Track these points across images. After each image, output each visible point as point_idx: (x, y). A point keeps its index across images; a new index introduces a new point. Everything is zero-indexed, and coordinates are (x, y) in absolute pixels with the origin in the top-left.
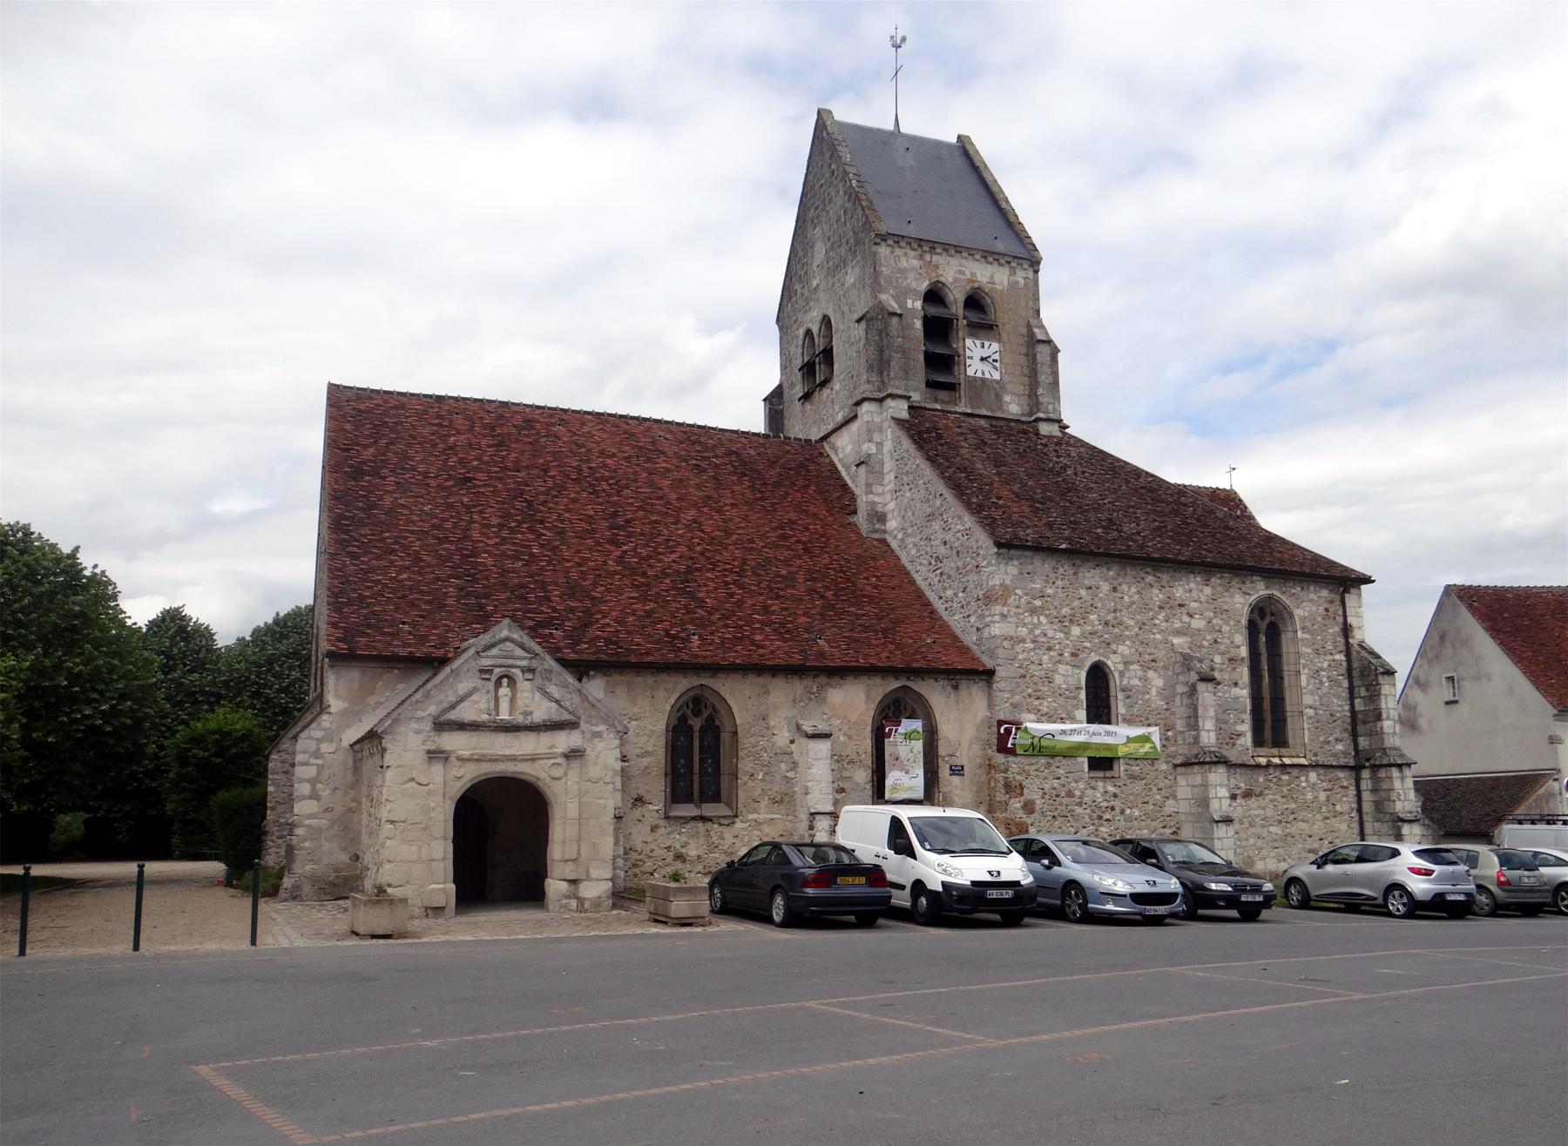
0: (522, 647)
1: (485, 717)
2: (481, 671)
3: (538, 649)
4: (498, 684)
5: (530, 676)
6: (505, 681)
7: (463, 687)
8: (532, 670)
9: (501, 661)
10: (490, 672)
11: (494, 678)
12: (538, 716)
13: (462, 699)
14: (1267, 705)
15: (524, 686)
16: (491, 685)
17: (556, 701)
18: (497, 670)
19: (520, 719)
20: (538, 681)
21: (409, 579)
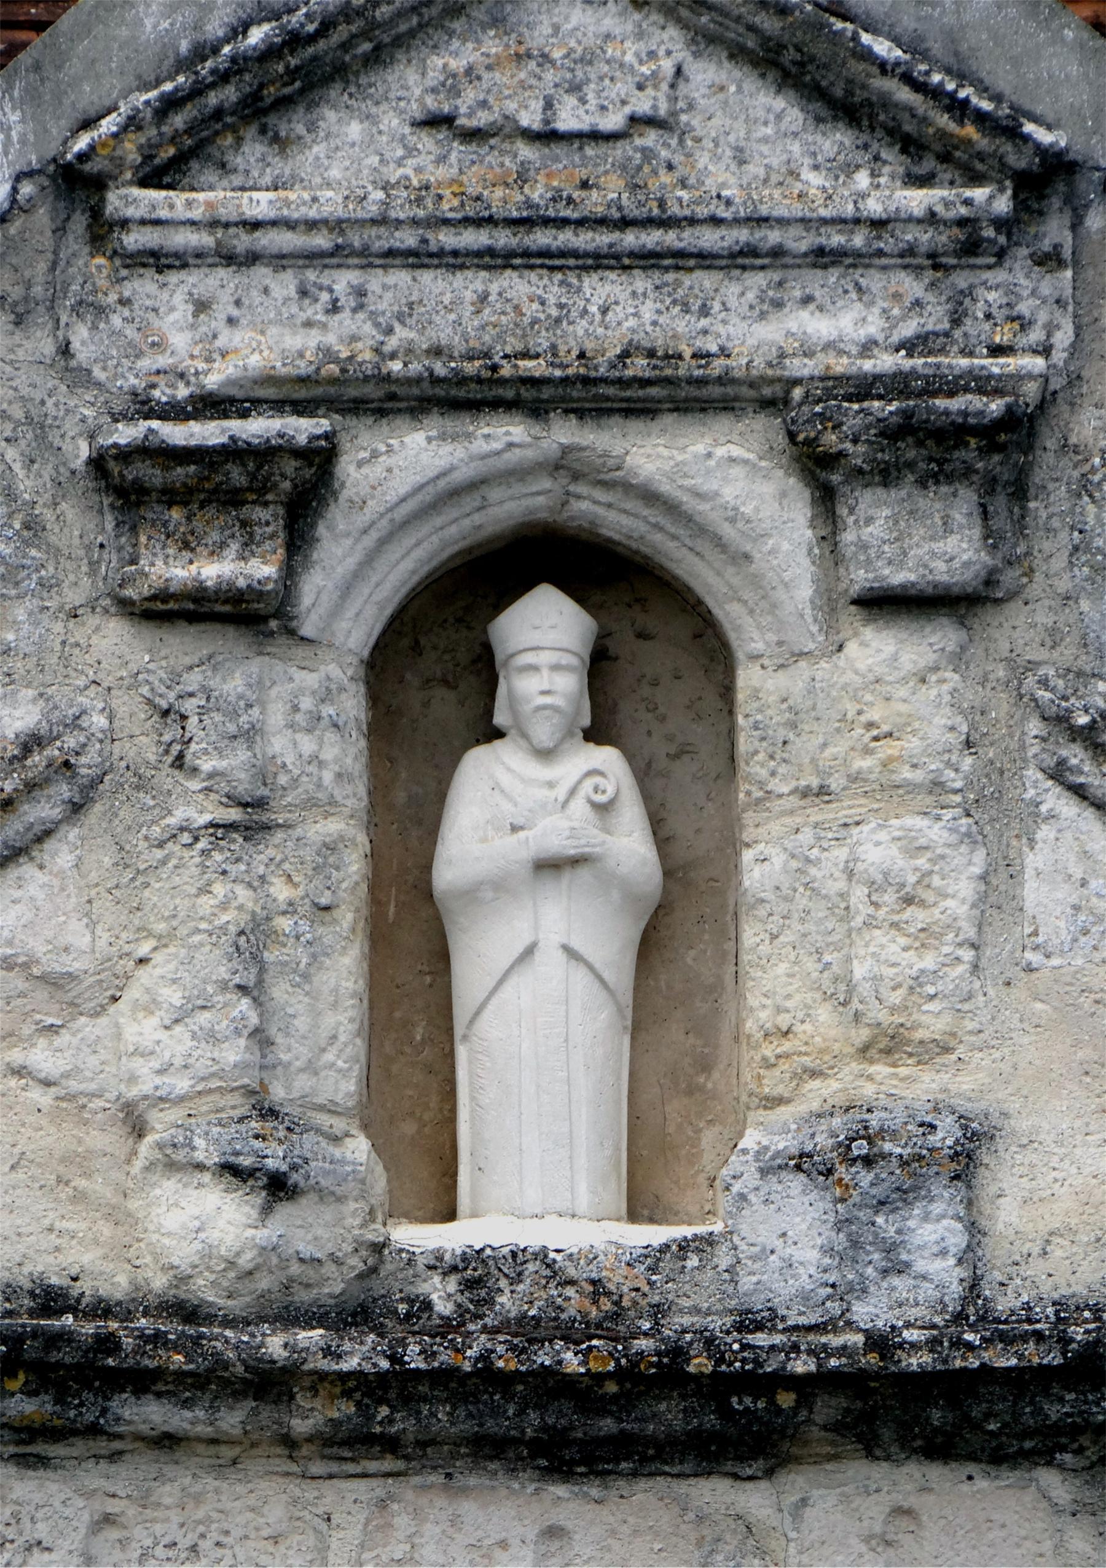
1: (194, 1231)
2: (135, 486)
4: (431, 677)
6: (544, 637)
8: (975, 448)
9: (454, 313)
10: (296, 492)
11: (351, 588)
14: (670, 238)
15: (841, 704)
16: (302, 710)
18: (395, 465)
19: (780, 1251)
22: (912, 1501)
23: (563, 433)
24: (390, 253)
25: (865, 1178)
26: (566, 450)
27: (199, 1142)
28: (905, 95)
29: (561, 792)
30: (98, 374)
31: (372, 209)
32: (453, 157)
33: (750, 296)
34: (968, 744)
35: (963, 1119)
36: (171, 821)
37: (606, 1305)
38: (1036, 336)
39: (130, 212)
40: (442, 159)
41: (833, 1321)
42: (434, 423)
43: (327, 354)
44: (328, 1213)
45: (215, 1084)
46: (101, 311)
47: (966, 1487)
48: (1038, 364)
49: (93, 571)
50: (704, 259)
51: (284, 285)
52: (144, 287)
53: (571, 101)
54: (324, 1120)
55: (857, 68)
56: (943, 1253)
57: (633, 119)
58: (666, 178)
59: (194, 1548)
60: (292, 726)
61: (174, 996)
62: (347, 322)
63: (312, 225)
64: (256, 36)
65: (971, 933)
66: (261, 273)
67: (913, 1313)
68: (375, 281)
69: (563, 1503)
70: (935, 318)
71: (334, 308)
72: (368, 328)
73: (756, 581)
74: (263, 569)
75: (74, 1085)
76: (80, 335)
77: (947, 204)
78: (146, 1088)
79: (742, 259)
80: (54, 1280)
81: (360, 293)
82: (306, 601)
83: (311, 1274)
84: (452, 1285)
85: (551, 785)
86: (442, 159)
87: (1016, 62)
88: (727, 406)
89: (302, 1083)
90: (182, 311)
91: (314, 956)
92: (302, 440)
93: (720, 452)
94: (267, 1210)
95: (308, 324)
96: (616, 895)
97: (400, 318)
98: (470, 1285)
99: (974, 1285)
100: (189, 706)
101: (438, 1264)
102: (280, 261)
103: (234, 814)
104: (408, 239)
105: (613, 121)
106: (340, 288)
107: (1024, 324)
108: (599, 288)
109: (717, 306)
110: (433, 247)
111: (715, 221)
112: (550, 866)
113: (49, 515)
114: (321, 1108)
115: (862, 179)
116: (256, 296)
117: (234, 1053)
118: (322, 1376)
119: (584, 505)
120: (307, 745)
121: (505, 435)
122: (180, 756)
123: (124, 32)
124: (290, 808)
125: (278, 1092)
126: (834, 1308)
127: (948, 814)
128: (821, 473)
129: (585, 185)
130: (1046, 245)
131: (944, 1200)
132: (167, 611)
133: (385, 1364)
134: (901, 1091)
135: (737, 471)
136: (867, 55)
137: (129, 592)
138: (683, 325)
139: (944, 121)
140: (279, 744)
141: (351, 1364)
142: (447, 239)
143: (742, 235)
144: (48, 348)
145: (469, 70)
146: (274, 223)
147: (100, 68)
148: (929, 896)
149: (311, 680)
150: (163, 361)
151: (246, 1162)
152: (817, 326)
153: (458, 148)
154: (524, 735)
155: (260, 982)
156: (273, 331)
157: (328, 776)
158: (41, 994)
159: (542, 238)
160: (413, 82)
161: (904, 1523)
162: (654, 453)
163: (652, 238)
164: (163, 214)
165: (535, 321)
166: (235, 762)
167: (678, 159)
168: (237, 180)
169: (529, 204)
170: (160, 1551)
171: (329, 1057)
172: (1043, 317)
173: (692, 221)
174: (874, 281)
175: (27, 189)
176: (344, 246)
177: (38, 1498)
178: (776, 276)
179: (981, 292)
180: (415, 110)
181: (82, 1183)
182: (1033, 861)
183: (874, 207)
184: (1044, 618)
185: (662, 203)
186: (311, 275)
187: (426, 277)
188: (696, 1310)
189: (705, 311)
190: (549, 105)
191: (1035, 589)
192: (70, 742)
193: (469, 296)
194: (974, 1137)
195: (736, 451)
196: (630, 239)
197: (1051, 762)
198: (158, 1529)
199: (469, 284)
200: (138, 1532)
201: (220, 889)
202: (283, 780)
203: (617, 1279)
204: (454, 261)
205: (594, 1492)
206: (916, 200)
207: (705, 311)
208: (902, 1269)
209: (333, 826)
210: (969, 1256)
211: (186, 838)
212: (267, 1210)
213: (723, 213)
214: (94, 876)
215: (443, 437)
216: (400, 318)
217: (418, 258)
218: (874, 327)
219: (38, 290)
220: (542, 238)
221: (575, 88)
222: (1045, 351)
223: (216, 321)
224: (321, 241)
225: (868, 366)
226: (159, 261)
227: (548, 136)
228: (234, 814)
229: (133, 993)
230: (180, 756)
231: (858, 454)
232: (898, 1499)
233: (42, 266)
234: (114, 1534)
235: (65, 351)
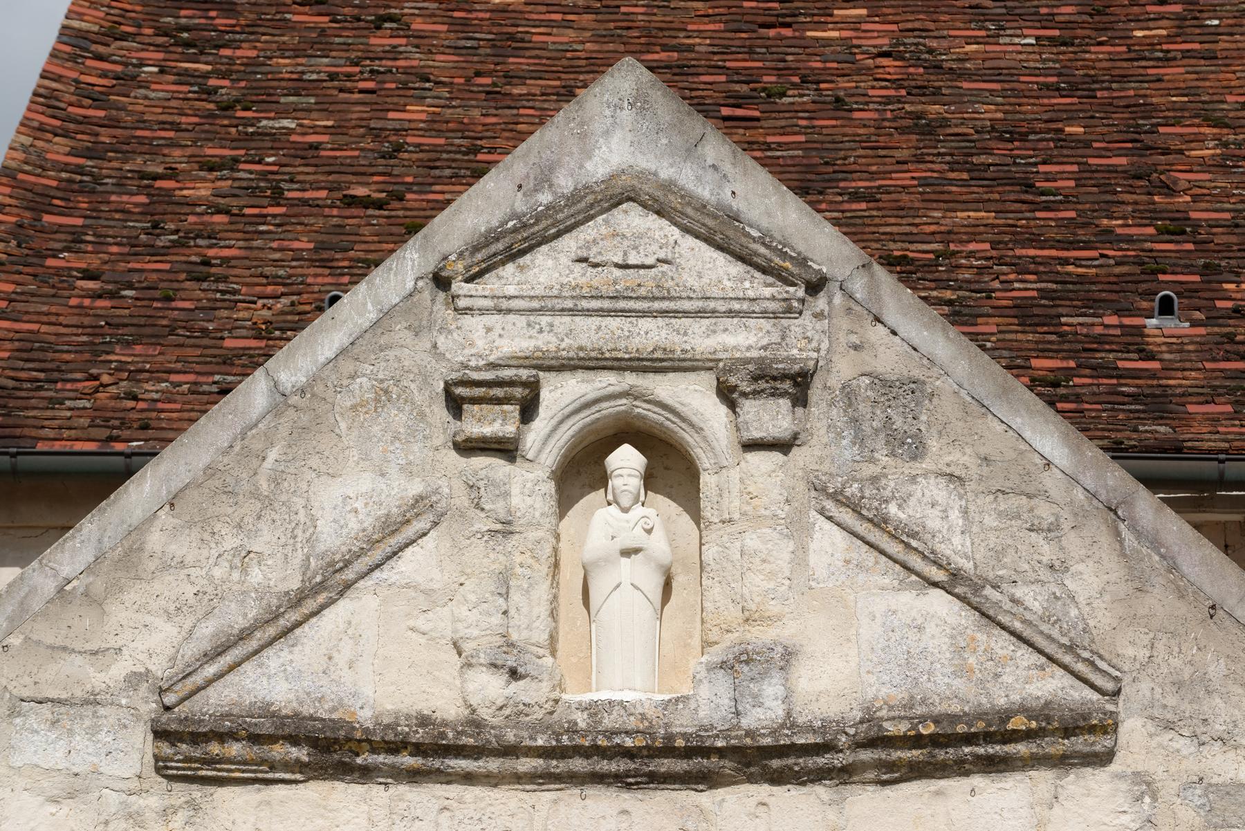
0: (721, 232)
3: (820, 241)
5: (770, 417)
6: (626, 461)
7: (345, 497)
9: (589, 333)
11: (546, 439)
12: (831, 683)
13: (329, 583)
17: (954, 582)
20: (827, 445)
21: (434, 125)
22: (766, 800)
23: (630, 379)
24: (563, 310)
25: (746, 669)
26: (632, 387)
27: (482, 655)
28: (762, 250)
29: (632, 525)
30: (448, 356)
31: (555, 292)
32: (588, 274)
33: (703, 329)
34: (787, 501)
35: (786, 648)
36: (474, 529)
37: (647, 724)
38: (814, 344)
39: (460, 292)
40: (584, 275)
41: (734, 726)
42: (580, 374)
43: (538, 349)
44: (534, 685)
45: (489, 632)
46: (450, 332)
47: (787, 794)
48: (815, 355)
49: (444, 433)
50: (686, 314)
51: (521, 321)
52: (467, 320)
53: (634, 252)
54: (535, 649)
55: (744, 240)
56: (776, 699)
57: (658, 260)
58: (671, 283)
59: (480, 819)
60: (522, 493)
61: (472, 598)
62: (546, 337)
63: (532, 297)
64: (511, 224)
65: (787, 574)
66: (511, 317)
67: (765, 723)
68: (557, 320)
69: (627, 799)
70: (776, 338)
71: (541, 331)
72: (554, 339)
73: (705, 438)
74: (510, 429)
75: (434, 634)
76: (441, 340)
77: (780, 293)
78: (461, 634)
79: (699, 314)
80: (425, 712)
81: (551, 325)
82: (528, 445)
83: (527, 710)
84: (585, 716)
85: (628, 522)
86: (584, 275)
87: (806, 239)
88: (693, 369)
89: (525, 634)
90: (482, 332)
91: (531, 585)
92: (524, 378)
93: (691, 387)
94: (508, 683)
95: (530, 337)
96: (653, 565)
97: (567, 335)
98: (590, 715)
99: (789, 714)
100: (481, 484)
101: (582, 708)
102: (519, 311)
103: (499, 527)
104: (569, 304)
105: (650, 261)
106: (543, 324)
107: (810, 341)
108: (646, 324)
109: (690, 332)
110: (580, 308)
111: (690, 298)
112: (627, 553)
113: (427, 410)
114: (533, 645)
115: (747, 284)
116: (509, 327)
117: (497, 619)
118: (530, 748)
119: (639, 410)
120: (529, 501)
121: (608, 381)
122: (478, 504)
123: (460, 224)
124: (521, 525)
125: (514, 637)
126: (735, 721)
127: (779, 528)
128: (727, 394)
129: (639, 285)
130: (818, 310)
131: (777, 678)
132: (469, 447)
133: (554, 743)
134: (760, 635)
135: (697, 395)
136: (748, 235)
137: (458, 439)
138: (677, 339)
139: (777, 260)
140: (516, 501)
141: (540, 742)
142: (584, 304)
143: (700, 304)
144: (429, 345)
145: (594, 240)
146: (516, 297)
147: (450, 237)
148: (772, 559)
149: (530, 476)
150: (473, 351)
151: (499, 662)
152: (730, 340)
153: (590, 269)
154: (618, 504)
155: (507, 593)
156: (517, 340)
157: (537, 514)
158: (422, 597)
159: (622, 304)
160: (570, 244)
161: (762, 808)
162: (665, 387)
163: (665, 305)
164: (474, 293)
165: (619, 337)
166: (499, 507)
167: (676, 276)
168: (503, 282)
169: (617, 291)
170: (466, 821)
171: (537, 624)
172: (816, 337)
173: (680, 298)
174: (751, 322)
175: (420, 283)
176: (543, 307)
177: (418, 799)
178: (713, 320)
179: (792, 328)
180: (573, 256)
181: (437, 673)
182: (813, 546)
183: (751, 294)
184: (817, 453)
185: (669, 292)
186: (532, 318)
187: (577, 319)
188: (682, 725)
189: (685, 334)
190: (625, 254)
191: (813, 442)
192: (434, 499)
193: (594, 327)
194: (790, 654)
195: (697, 387)
196: (657, 305)
197: (819, 507)
198: (466, 811)
199: (595, 321)
200: (457, 813)
201: (492, 556)
202: (518, 514)
203: (651, 713)
204: (588, 313)
205: (640, 797)
206: (768, 292)
207: (685, 334)
208: (761, 705)
209: (540, 534)
210: (786, 699)
211: (479, 536)
212: (508, 683)
213: (692, 295)
214: (442, 551)
215: (583, 381)
216: (567, 335)
217: (573, 312)
218: (752, 340)
219: (424, 323)
220: (622, 304)
221: (635, 248)
222: (818, 350)
223: (494, 335)
224: (535, 304)
225: (748, 355)
226: (468, 310)
227: (626, 267)
228: (499, 527)
229: (458, 597)
230: (478, 504)
231: (745, 387)
232: (760, 799)
233: (426, 314)
234: (447, 814)
235: (435, 346)
